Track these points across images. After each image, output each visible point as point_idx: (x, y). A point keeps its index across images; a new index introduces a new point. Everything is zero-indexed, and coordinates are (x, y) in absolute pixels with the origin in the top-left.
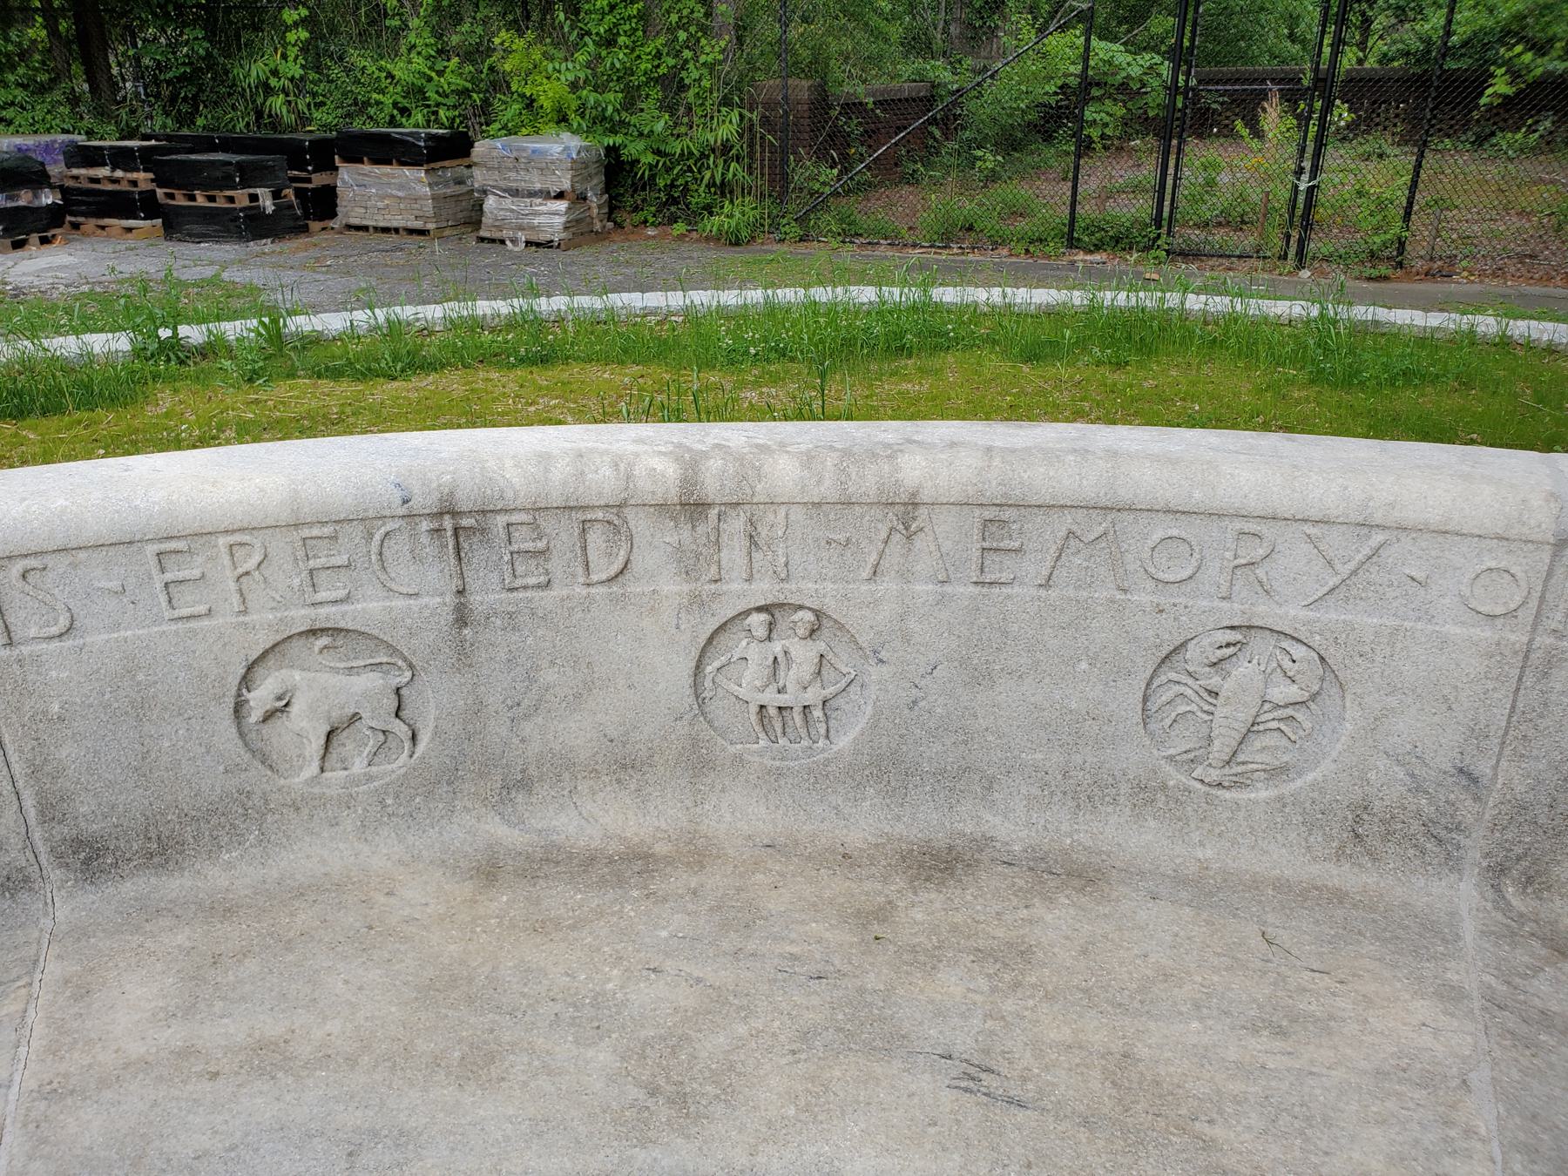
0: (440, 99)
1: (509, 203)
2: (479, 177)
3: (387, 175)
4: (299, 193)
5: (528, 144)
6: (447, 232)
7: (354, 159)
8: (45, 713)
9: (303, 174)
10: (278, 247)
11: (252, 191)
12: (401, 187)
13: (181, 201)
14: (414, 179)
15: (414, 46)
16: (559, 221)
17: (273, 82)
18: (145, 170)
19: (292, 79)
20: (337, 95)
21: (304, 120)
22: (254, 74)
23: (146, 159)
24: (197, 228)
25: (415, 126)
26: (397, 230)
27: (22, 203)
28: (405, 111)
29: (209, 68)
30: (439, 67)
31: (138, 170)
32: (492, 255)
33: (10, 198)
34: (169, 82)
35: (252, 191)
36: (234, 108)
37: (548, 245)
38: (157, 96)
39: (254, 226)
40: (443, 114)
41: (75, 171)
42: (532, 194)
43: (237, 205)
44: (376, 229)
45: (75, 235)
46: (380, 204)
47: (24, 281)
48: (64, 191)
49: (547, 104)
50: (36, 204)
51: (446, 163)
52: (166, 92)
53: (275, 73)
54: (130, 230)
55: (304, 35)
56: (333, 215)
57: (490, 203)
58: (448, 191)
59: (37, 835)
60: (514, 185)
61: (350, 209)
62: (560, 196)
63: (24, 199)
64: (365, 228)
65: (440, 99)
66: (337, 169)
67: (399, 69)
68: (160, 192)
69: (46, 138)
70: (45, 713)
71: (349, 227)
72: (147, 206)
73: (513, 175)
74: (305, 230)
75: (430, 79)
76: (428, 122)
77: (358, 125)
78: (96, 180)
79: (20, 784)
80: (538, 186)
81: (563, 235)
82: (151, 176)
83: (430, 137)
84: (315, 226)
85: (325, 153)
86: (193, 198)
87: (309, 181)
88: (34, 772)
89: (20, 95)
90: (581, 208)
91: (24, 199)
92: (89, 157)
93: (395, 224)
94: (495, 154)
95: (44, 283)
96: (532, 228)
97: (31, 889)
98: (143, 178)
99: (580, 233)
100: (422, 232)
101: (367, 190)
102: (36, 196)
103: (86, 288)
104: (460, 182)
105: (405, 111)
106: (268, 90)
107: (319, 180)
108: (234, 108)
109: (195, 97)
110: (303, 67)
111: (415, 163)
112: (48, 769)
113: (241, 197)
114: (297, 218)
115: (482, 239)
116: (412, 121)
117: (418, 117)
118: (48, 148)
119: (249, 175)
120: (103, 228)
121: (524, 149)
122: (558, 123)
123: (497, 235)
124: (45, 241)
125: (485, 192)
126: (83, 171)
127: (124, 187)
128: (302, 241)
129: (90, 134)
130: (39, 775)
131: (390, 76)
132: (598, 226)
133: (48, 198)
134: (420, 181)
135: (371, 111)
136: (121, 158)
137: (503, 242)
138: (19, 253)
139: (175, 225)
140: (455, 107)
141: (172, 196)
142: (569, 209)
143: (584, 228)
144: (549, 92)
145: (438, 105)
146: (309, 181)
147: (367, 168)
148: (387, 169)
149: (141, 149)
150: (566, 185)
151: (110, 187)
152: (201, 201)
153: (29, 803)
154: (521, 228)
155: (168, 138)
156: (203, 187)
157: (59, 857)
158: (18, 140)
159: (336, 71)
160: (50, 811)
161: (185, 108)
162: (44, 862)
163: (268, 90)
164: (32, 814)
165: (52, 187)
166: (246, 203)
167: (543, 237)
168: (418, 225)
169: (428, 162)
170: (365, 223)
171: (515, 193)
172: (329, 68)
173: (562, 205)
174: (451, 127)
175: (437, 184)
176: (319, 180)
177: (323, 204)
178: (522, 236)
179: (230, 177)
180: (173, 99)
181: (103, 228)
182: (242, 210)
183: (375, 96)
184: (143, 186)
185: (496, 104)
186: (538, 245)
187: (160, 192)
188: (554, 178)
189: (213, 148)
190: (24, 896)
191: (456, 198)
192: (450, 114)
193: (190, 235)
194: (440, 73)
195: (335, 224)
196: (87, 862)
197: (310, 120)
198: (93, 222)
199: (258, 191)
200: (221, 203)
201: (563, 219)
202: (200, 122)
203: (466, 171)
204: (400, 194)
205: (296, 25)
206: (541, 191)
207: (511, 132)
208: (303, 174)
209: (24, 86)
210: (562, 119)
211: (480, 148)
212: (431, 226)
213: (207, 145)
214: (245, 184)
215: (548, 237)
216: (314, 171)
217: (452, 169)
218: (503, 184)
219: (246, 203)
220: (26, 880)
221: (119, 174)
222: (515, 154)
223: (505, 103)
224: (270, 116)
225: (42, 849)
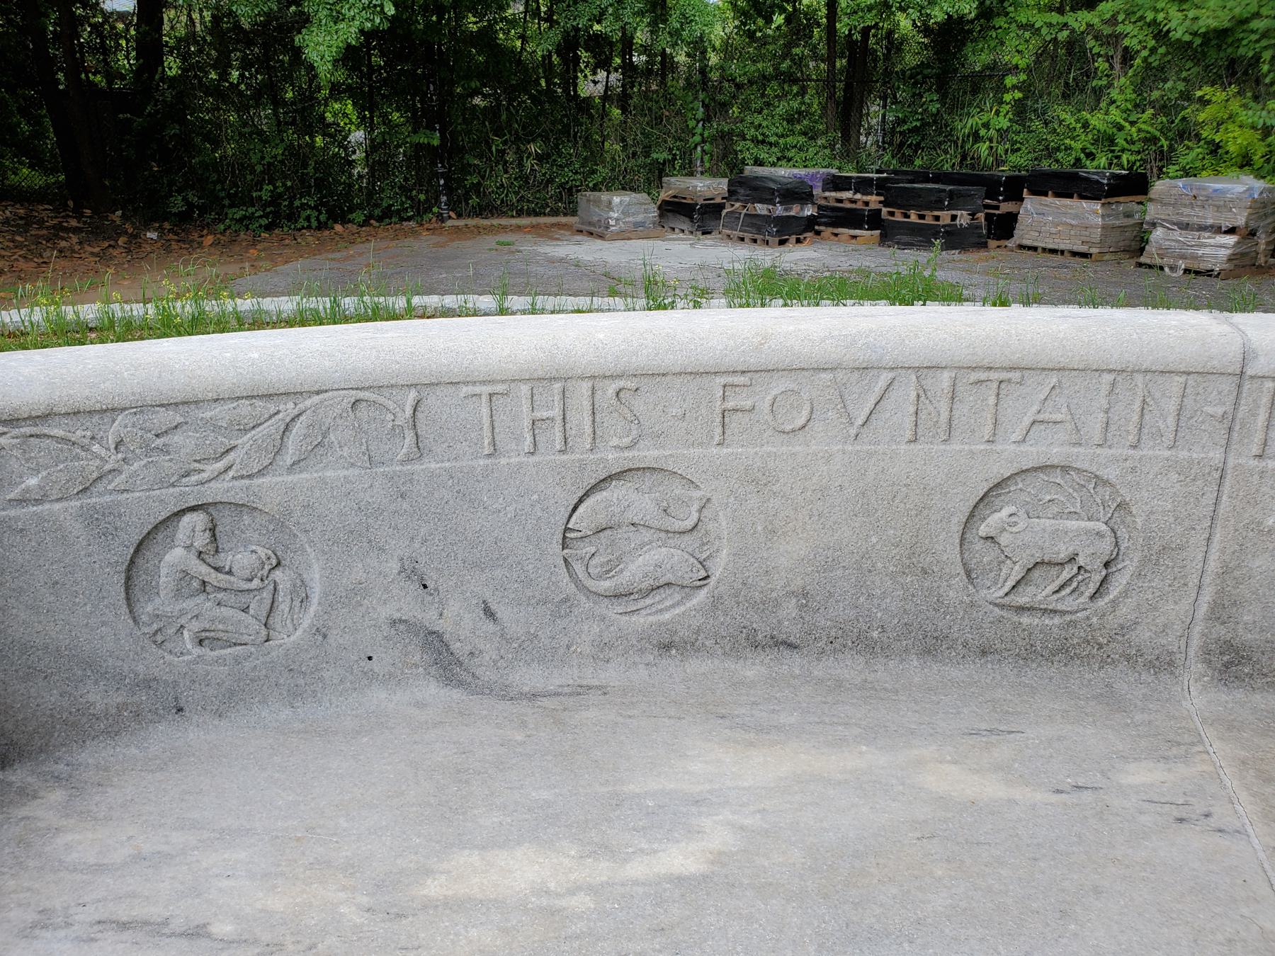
0: (1126, 146)
1: (1177, 235)
2: (1152, 211)
3: (1066, 206)
4: (988, 217)
5: (1211, 184)
6: (1107, 257)
7: (1039, 192)
8: (1260, 523)
9: (994, 203)
10: (963, 257)
11: (936, 213)
12: (1076, 216)
13: (898, 217)
14: (1090, 212)
15: (1114, 102)
16: (1224, 253)
17: (982, 132)
18: (878, 194)
19: (998, 131)
20: (1033, 142)
21: (999, 162)
22: (969, 125)
23: (880, 186)
24: (905, 239)
25: (1099, 167)
26: (1062, 252)
27: (792, 213)
28: (1090, 156)
29: (935, 122)
30: (1132, 118)
31: (871, 194)
32: (1150, 278)
33: (786, 210)
34: (901, 133)
35: (936, 213)
36: (946, 152)
37: (1208, 273)
38: (891, 144)
39: (956, 239)
40: (1125, 158)
41: (827, 194)
42: (1202, 228)
43: (941, 223)
44: (1044, 250)
45: (817, 238)
46: (1053, 230)
47: (787, 266)
48: (820, 207)
49: (1232, 148)
50: (801, 215)
51: (1121, 199)
52: (898, 139)
53: (986, 126)
54: (854, 237)
55: (1018, 95)
56: (1008, 234)
57: (1158, 234)
58: (1117, 223)
59: (1197, 629)
60: (1186, 219)
61: (1025, 232)
62: (1231, 231)
63: (795, 211)
64: (1035, 249)
65: (1126, 146)
66: (1022, 200)
67: (1097, 120)
68: (885, 210)
69: (811, 171)
70: (1260, 523)
71: (1021, 247)
72: (874, 220)
73: (1187, 211)
74: (984, 246)
75: (1121, 128)
76: (1110, 164)
77: (1045, 165)
78: (840, 201)
79: (1207, 580)
80: (1210, 222)
81: (1225, 266)
82: (882, 198)
83: (1114, 176)
84: (993, 243)
85: (1015, 188)
86: (907, 216)
87: (997, 208)
88: (1226, 571)
89: (802, 139)
90: (1250, 243)
91: (795, 211)
92: (836, 183)
93: (1062, 247)
94: (1173, 192)
95: (801, 268)
96: (1195, 257)
97: (1172, 673)
98: (874, 200)
99: (1243, 264)
100: (1084, 255)
101: (1041, 217)
102: (802, 209)
103: (827, 274)
104: (1128, 215)
105: (1090, 156)
106: (977, 137)
107: (1006, 207)
108: (946, 152)
109: (918, 144)
110: (1010, 120)
111: (1096, 198)
112: (1237, 573)
113: (945, 217)
114: (980, 236)
115: (1140, 265)
116: (1095, 163)
117: (1103, 161)
118: (813, 177)
119: (955, 201)
120: (836, 235)
121: (1204, 189)
122: (1241, 167)
123: (1158, 261)
124: (798, 241)
125: (1154, 225)
126: (833, 194)
127: (859, 206)
128: (983, 254)
129: (839, 168)
130: (1226, 577)
131: (1086, 125)
132: (1262, 260)
133: (809, 211)
134: (1095, 212)
135: (1060, 155)
136: (863, 186)
137: (1162, 268)
138: (782, 248)
139: (889, 234)
140: (1138, 152)
141: (892, 214)
142: (1238, 243)
143: (1247, 261)
144: (1235, 139)
145: (1123, 150)
146: (997, 208)
147: (1050, 199)
148: (1067, 201)
149: (878, 179)
150: (1240, 221)
151: (849, 206)
152: (913, 218)
153: (1207, 597)
154: (1183, 257)
155: (895, 172)
156: (918, 207)
157: (1206, 654)
158: (796, 171)
159: (1037, 124)
160: (1219, 612)
161: (908, 152)
162: (1192, 653)
163: (977, 137)
164: (1203, 609)
165: (813, 204)
166: (948, 221)
167: (1203, 266)
168: (1083, 249)
169: (1106, 197)
170: (1035, 244)
171: (1185, 227)
172: (1031, 120)
173: (1231, 240)
174: (1130, 169)
175: (1109, 216)
176: (1006, 207)
177: (1004, 227)
178: (1182, 265)
179: (942, 202)
180: (901, 145)
181: (836, 235)
182: (944, 226)
183: (1067, 141)
184: (873, 206)
185: (1180, 149)
186: (1197, 273)
187: (885, 210)
188: (1229, 215)
189: (927, 180)
190: (1164, 677)
191: (1122, 228)
192: (1132, 158)
193: (898, 243)
194: (1132, 123)
195: (1011, 243)
196: (1227, 665)
197: (1004, 162)
198: (830, 230)
199: (959, 213)
200: (929, 221)
201: (1229, 252)
202: (918, 162)
203: (1136, 207)
204: (1073, 222)
205: (1014, 87)
206: (1212, 226)
207: (1186, 173)
208: (994, 203)
209: (805, 134)
210: (1245, 162)
211: (1159, 187)
212: (1094, 251)
213: (923, 177)
214: (949, 208)
215: (1209, 266)
216: (1004, 201)
217: (1127, 204)
218: (1174, 218)
219: (948, 221)
220: (1171, 663)
221: (858, 196)
222: (1195, 192)
223: (1188, 148)
224: (973, 158)
225: (1196, 642)
